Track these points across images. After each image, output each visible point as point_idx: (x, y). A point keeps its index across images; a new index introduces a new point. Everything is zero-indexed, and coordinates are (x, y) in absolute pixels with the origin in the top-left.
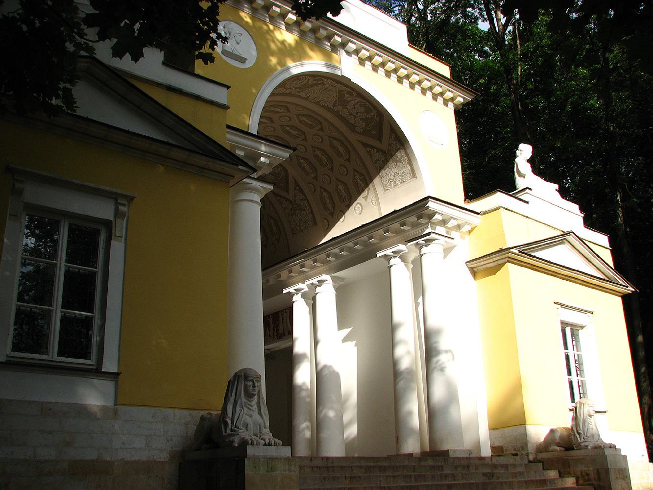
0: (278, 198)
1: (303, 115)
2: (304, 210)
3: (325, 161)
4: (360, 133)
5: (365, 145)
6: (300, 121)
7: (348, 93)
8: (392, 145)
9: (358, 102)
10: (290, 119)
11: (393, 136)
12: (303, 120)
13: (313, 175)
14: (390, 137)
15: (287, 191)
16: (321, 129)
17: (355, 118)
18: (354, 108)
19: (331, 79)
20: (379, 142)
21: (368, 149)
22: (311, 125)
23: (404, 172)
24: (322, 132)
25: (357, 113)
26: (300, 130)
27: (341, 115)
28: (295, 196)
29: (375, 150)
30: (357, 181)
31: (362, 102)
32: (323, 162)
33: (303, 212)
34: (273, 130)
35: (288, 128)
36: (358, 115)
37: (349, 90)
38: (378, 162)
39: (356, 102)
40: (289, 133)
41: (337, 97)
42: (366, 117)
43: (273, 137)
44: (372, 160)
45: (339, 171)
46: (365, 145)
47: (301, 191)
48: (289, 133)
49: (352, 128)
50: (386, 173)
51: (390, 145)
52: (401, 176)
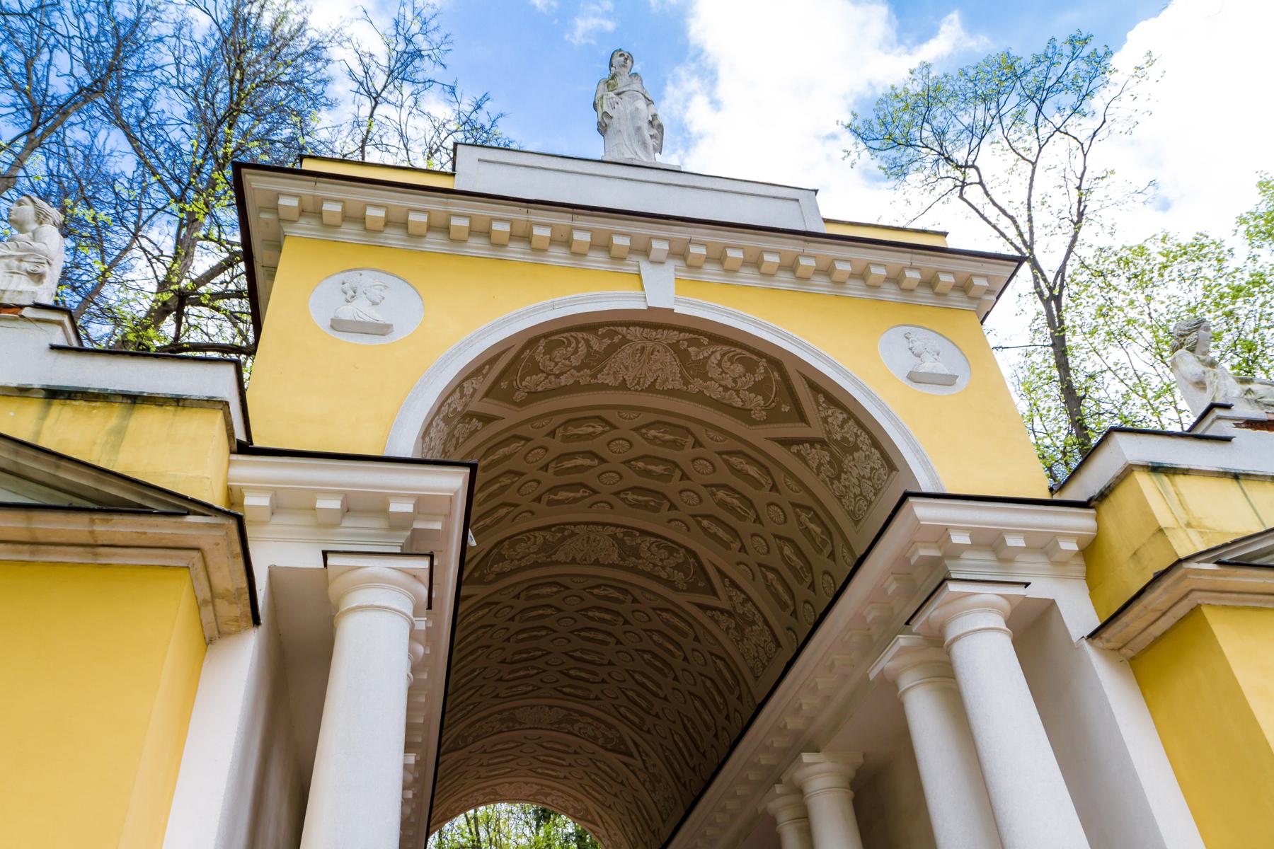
0: (709, 612)
1: (649, 426)
2: (856, 448)
3: (739, 507)
4: (764, 422)
5: (703, 607)
6: (653, 441)
7: (692, 342)
8: (830, 420)
9: (723, 356)
10: (621, 477)
11: (821, 398)
12: (655, 437)
13: (736, 545)
14: (818, 404)
15: (803, 418)
16: (697, 443)
17: (737, 392)
18: (723, 372)
19: (635, 324)
20: (804, 424)
21: (795, 448)
22: (675, 441)
23: (872, 469)
24: (677, 512)
25: (735, 380)
26: (666, 460)
27: (710, 397)
28: (731, 598)
29: (807, 445)
30: (807, 528)
31: (656, 542)
32: (739, 510)
33: (856, 455)
34: (617, 477)
35: (640, 464)
36: (739, 384)
37: (688, 336)
38: (822, 468)
39: (719, 358)
40: (648, 473)
41: (678, 360)
42: (754, 381)
43: (630, 493)
44: (811, 469)
45: (755, 548)
46: (786, 443)
47: (734, 584)
48: (648, 473)
49: (743, 414)
50: (845, 486)
51: (825, 420)
52: (870, 479)
